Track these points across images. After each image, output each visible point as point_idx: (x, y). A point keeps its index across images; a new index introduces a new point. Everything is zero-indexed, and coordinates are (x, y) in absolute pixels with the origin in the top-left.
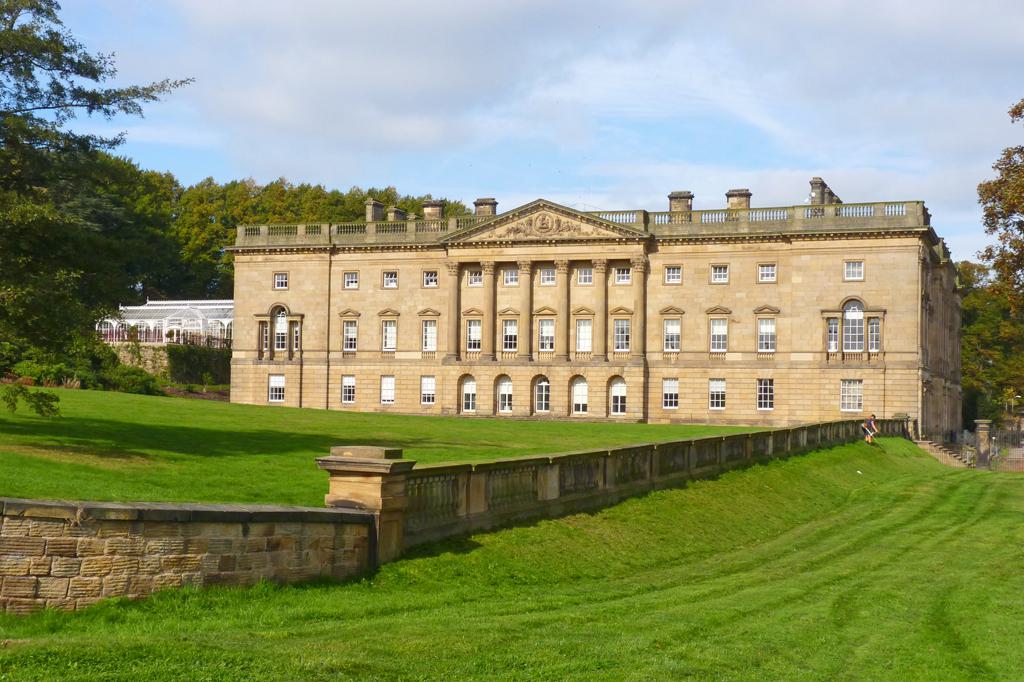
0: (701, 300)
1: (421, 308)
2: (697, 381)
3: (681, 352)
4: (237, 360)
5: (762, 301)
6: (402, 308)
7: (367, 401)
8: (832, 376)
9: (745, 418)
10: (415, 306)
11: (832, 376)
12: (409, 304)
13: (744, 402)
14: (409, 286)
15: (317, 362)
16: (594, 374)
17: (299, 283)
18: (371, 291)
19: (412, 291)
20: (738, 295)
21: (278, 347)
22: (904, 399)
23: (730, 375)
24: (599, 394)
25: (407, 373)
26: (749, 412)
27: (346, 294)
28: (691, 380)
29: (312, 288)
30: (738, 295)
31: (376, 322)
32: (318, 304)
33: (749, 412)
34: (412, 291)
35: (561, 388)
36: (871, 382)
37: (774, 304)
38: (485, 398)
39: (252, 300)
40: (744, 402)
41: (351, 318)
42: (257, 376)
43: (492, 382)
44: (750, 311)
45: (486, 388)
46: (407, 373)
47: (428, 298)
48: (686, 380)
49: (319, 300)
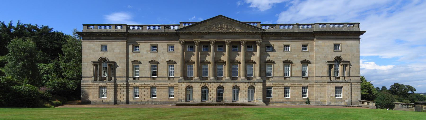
0: (280, 57)
1: (167, 60)
2: (279, 87)
3: (140, 77)
4: (362, 56)
5: (303, 58)
6: (159, 60)
7: (145, 97)
8: (332, 85)
10: (165, 59)
11: (332, 85)
12: (162, 58)
13: (298, 95)
15: (122, 82)
17: (113, 49)
18: (145, 53)
19: (163, 53)
20: (294, 56)
21: (341, 96)
22: (356, 93)
25: (162, 85)
26: (299, 99)
27: (134, 54)
29: (119, 51)
30: (294, 56)
32: (121, 58)
33: (299, 99)
34: (163, 53)
35: (229, 91)
36: (346, 87)
37: (308, 59)
39: (91, 56)
40: (298, 95)
41: (137, 63)
42: (94, 87)
43: (200, 89)
44: (299, 62)
45: (198, 91)
47: (171, 56)
48: (276, 87)
49: (122, 56)
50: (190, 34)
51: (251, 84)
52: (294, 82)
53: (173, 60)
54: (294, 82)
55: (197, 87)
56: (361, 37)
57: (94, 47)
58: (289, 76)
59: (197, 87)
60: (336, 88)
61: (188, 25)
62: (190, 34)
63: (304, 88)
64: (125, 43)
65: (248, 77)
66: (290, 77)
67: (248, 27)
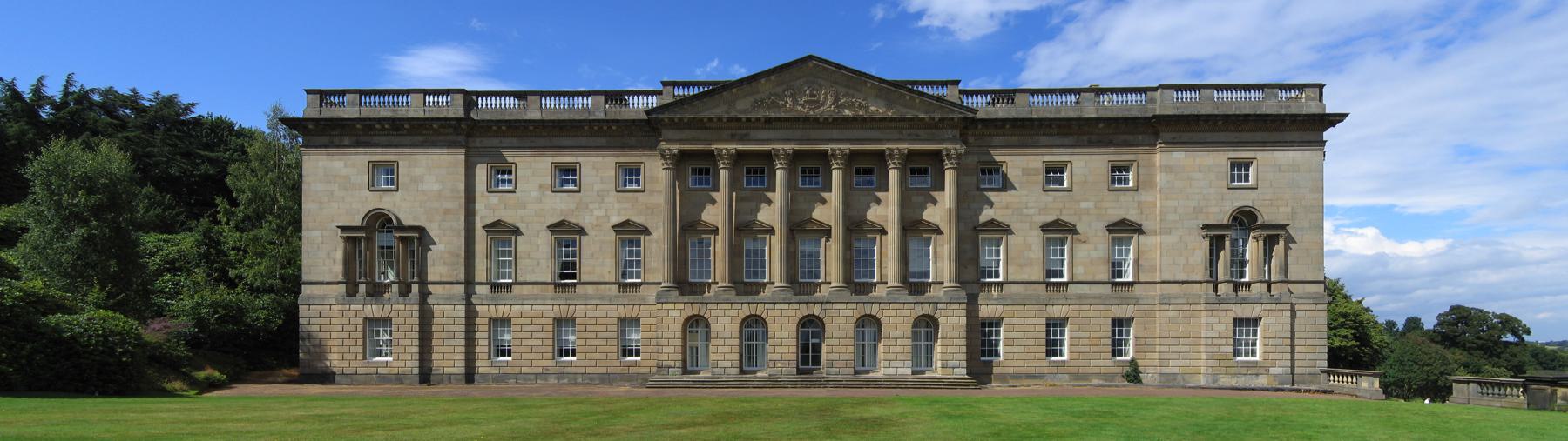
0: (1032, 211)
1: (616, 220)
2: (1029, 321)
3: (515, 283)
5: (1116, 214)
6: (585, 221)
7: (533, 356)
8: (1221, 313)
9: (1096, 370)
10: (607, 217)
11: (1221, 313)
12: (596, 213)
14: (596, 188)
15: (449, 300)
16: (894, 313)
17: (416, 180)
18: (534, 194)
19: (601, 195)
20: (1084, 205)
22: (1309, 342)
23: (1076, 314)
24: (729, 342)
25: (597, 314)
26: (1101, 363)
27: (494, 199)
28: (1021, 321)
29: (436, 187)
30: (1084, 205)
31: (1036, 239)
32: (447, 212)
33: (1101, 363)
34: (601, 195)
35: (843, 334)
36: (1273, 320)
37: (1133, 216)
38: (671, 350)
41: (503, 232)
42: (345, 321)
43: (737, 327)
44: (1101, 226)
45: (727, 335)
46: (597, 314)
48: (1015, 321)
49: (449, 205)
50: (698, 124)
51: (926, 309)
52: (1081, 301)
53: (1066, 218)
54: (1081, 301)
55: (726, 318)
56: (1328, 134)
57: (344, 172)
58: (1065, 279)
59: (726, 318)
60: (1238, 322)
61: (692, 92)
62: (698, 124)
63: (1119, 324)
64: (460, 157)
65: (914, 285)
66: (1066, 284)
67: (913, 99)
